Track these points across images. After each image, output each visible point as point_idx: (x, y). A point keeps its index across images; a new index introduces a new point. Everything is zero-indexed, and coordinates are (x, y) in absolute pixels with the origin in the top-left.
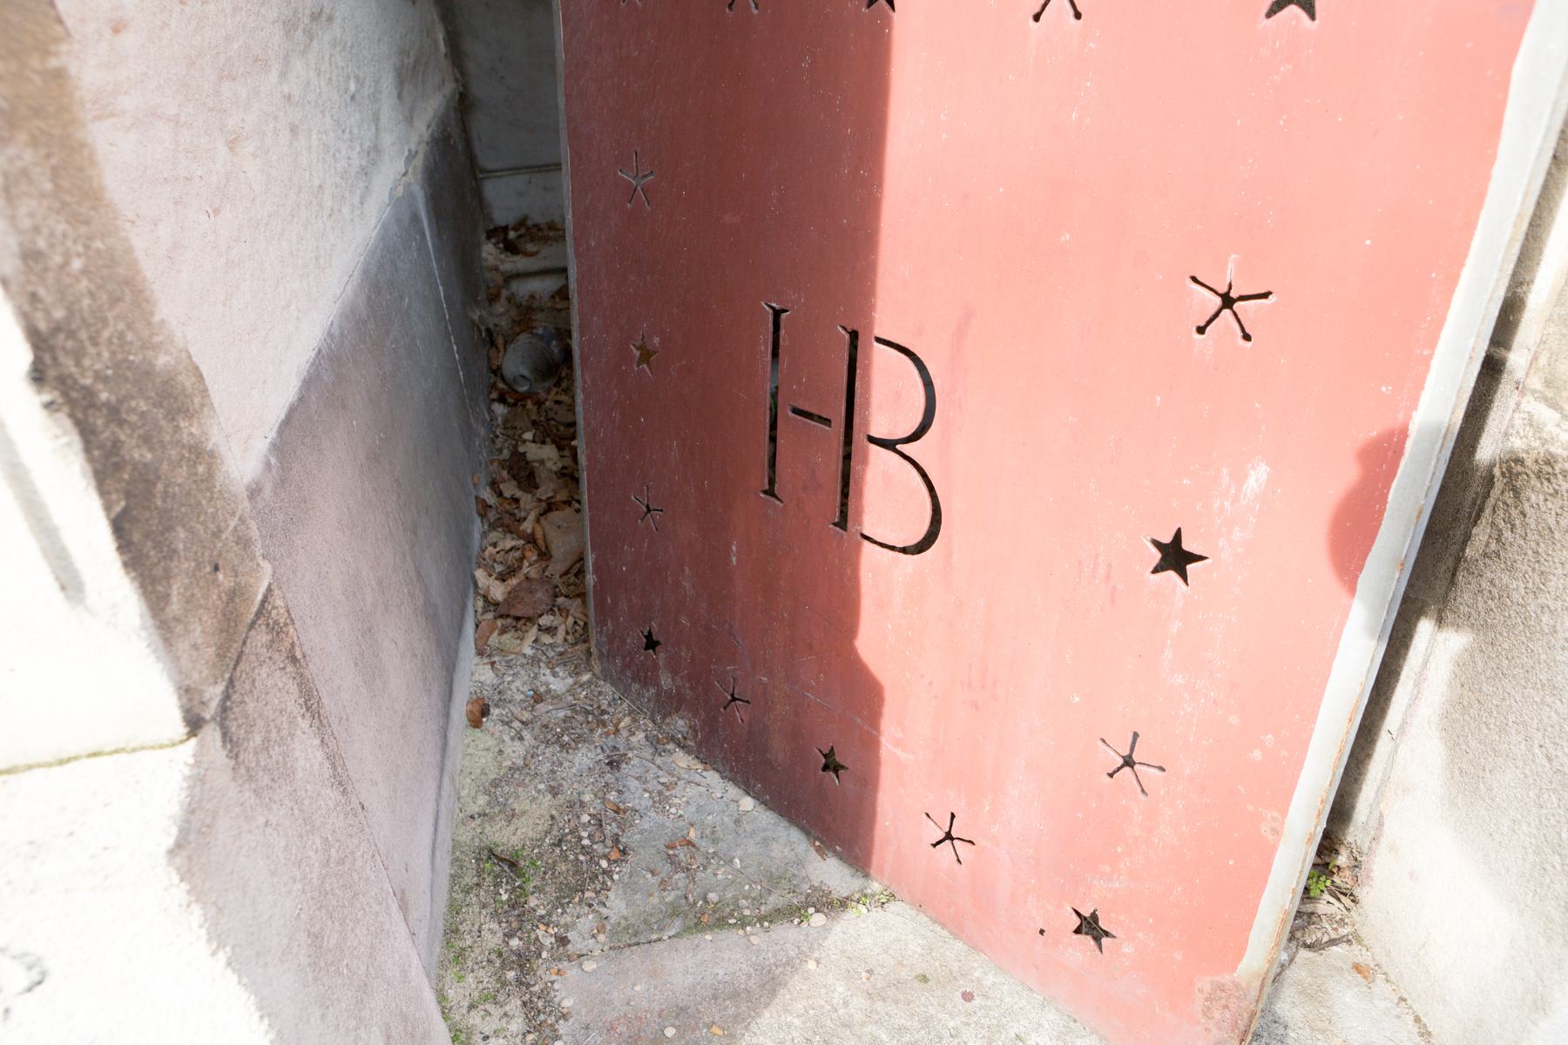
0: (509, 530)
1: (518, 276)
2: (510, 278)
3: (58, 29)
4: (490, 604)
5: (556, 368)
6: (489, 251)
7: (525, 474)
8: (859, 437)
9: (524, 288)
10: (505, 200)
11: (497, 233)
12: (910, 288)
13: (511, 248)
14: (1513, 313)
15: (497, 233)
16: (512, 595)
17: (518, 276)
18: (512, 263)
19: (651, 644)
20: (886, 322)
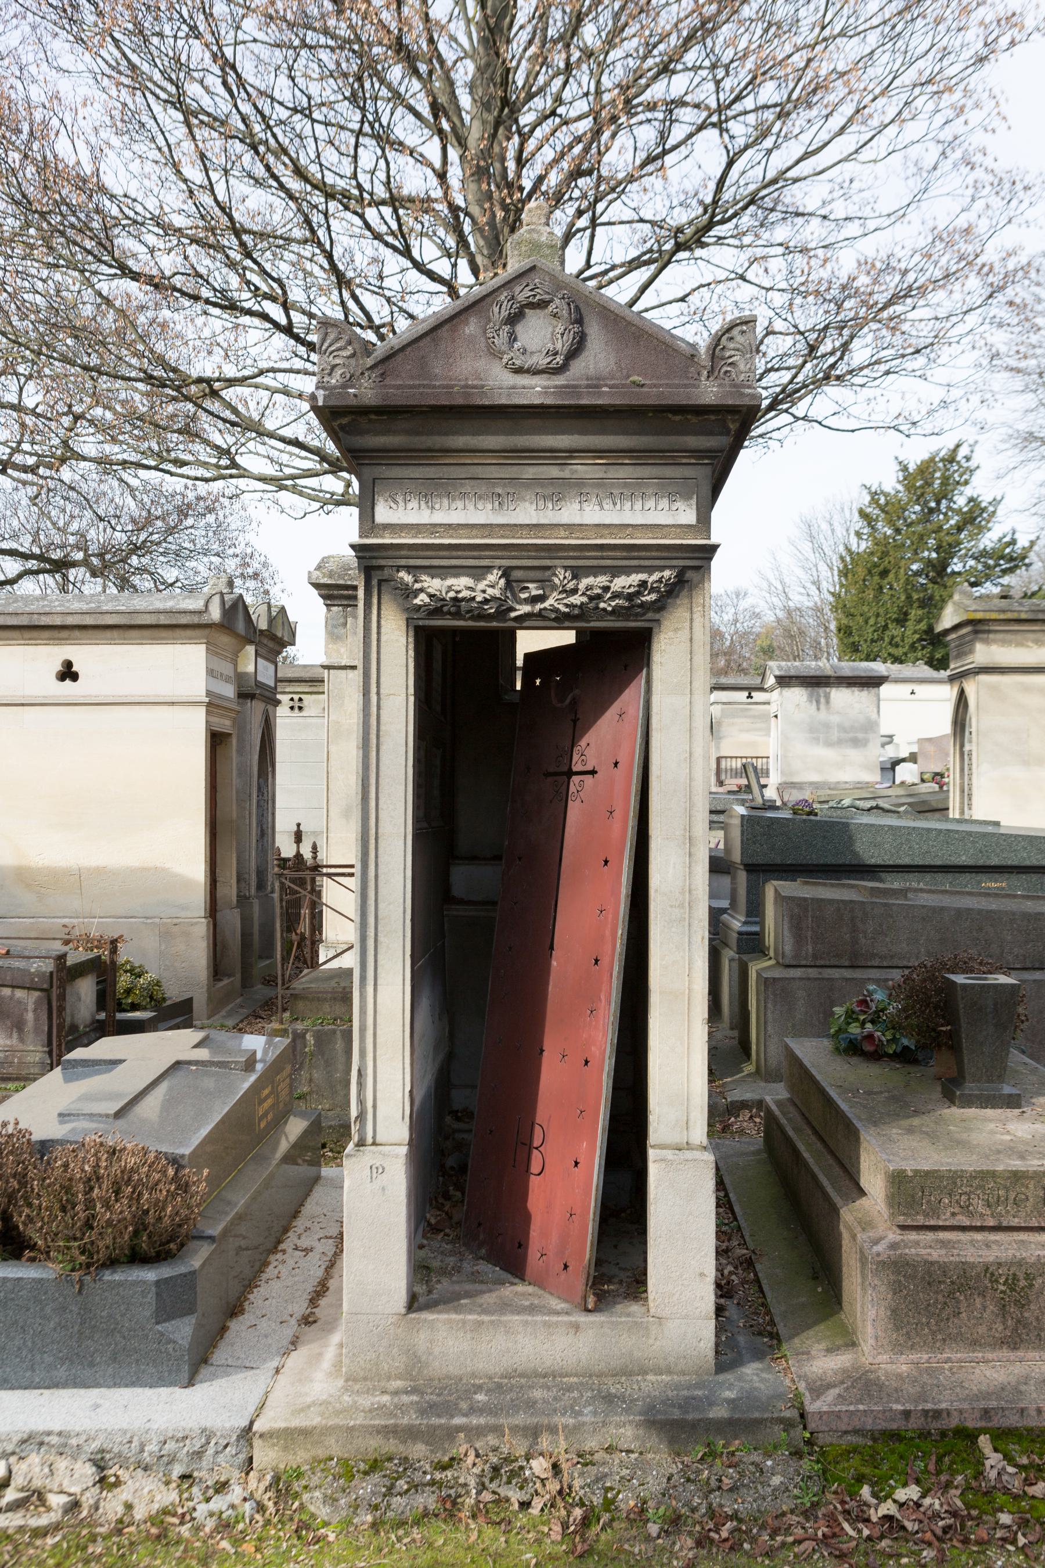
0: (439, 1209)
1: (460, 1131)
2: (455, 1131)
3: (230, 1023)
4: (429, 1224)
5: (463, 1169)
6: (448, 1119)
7: (447, 1196)
8: (358, 919)
9: (459, 1136)
10: (459, 1099)
11: (454, 1113)
12: (542, 1114)
13: (458, 1119)
14: (893, 1195)
15: (454, 1113)
16: (438, 1222)
17: (460, 1131)
18: (456, 1125)
19: (480, 1224)
20: (538, 1120)
